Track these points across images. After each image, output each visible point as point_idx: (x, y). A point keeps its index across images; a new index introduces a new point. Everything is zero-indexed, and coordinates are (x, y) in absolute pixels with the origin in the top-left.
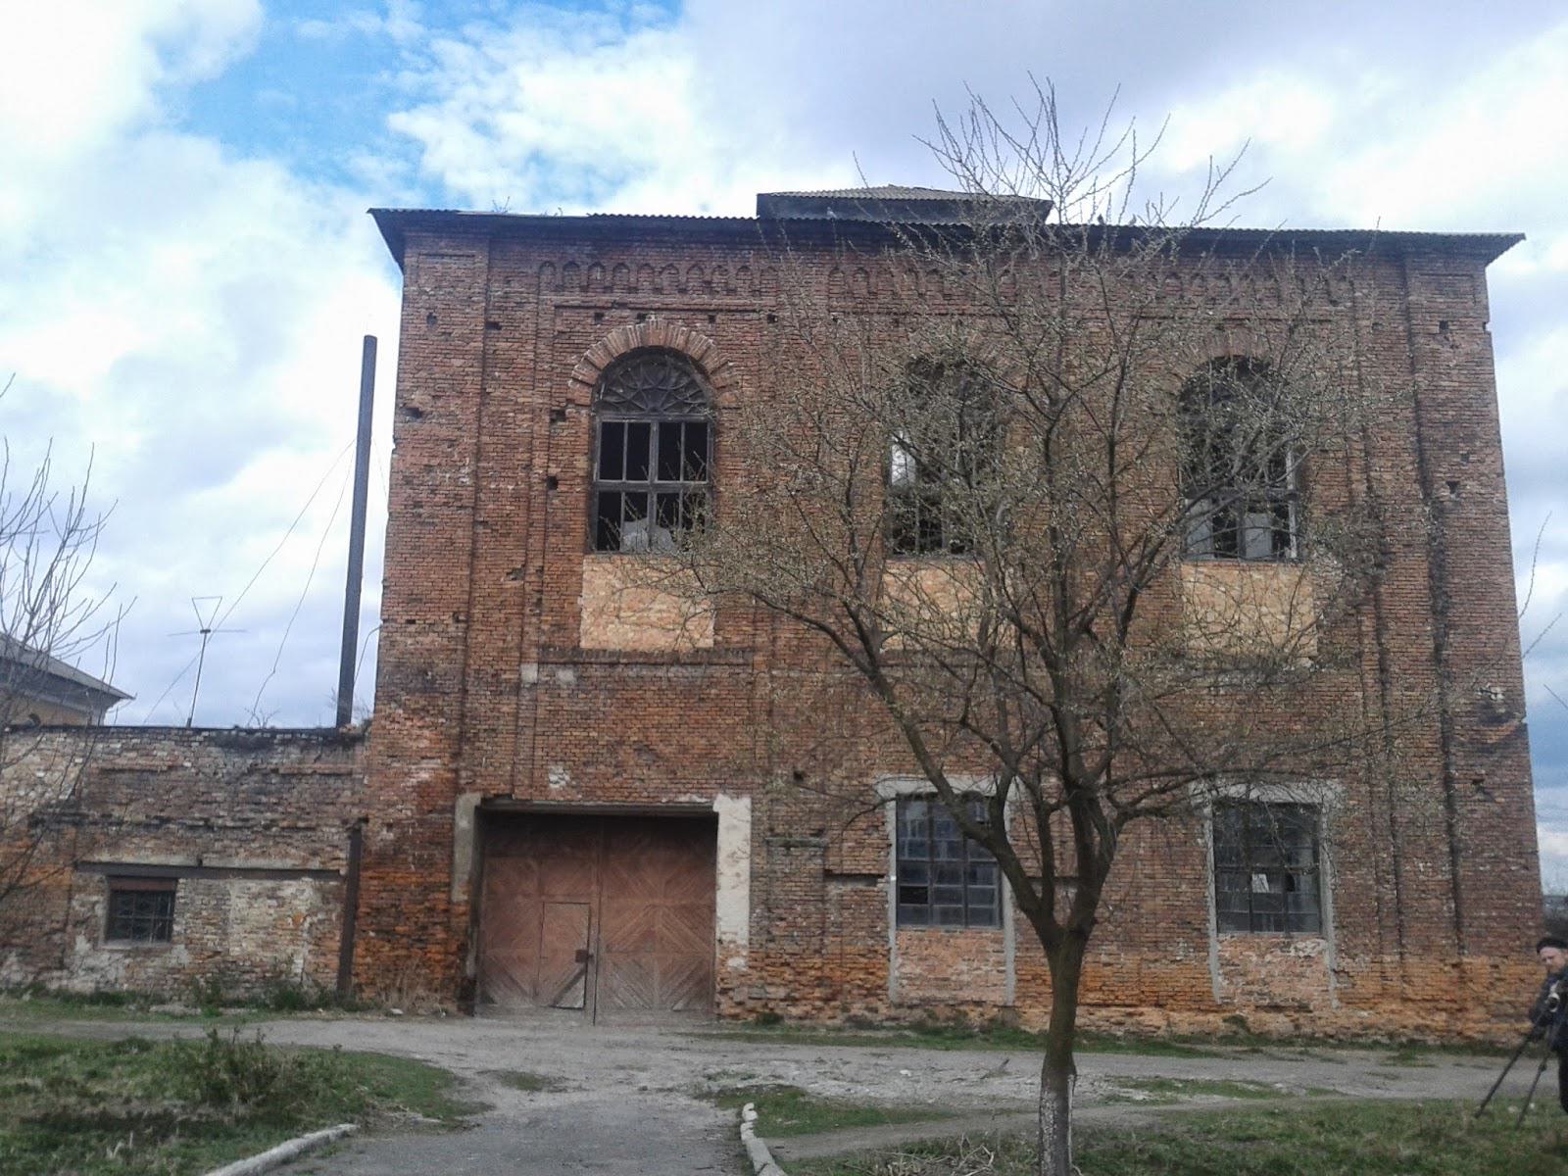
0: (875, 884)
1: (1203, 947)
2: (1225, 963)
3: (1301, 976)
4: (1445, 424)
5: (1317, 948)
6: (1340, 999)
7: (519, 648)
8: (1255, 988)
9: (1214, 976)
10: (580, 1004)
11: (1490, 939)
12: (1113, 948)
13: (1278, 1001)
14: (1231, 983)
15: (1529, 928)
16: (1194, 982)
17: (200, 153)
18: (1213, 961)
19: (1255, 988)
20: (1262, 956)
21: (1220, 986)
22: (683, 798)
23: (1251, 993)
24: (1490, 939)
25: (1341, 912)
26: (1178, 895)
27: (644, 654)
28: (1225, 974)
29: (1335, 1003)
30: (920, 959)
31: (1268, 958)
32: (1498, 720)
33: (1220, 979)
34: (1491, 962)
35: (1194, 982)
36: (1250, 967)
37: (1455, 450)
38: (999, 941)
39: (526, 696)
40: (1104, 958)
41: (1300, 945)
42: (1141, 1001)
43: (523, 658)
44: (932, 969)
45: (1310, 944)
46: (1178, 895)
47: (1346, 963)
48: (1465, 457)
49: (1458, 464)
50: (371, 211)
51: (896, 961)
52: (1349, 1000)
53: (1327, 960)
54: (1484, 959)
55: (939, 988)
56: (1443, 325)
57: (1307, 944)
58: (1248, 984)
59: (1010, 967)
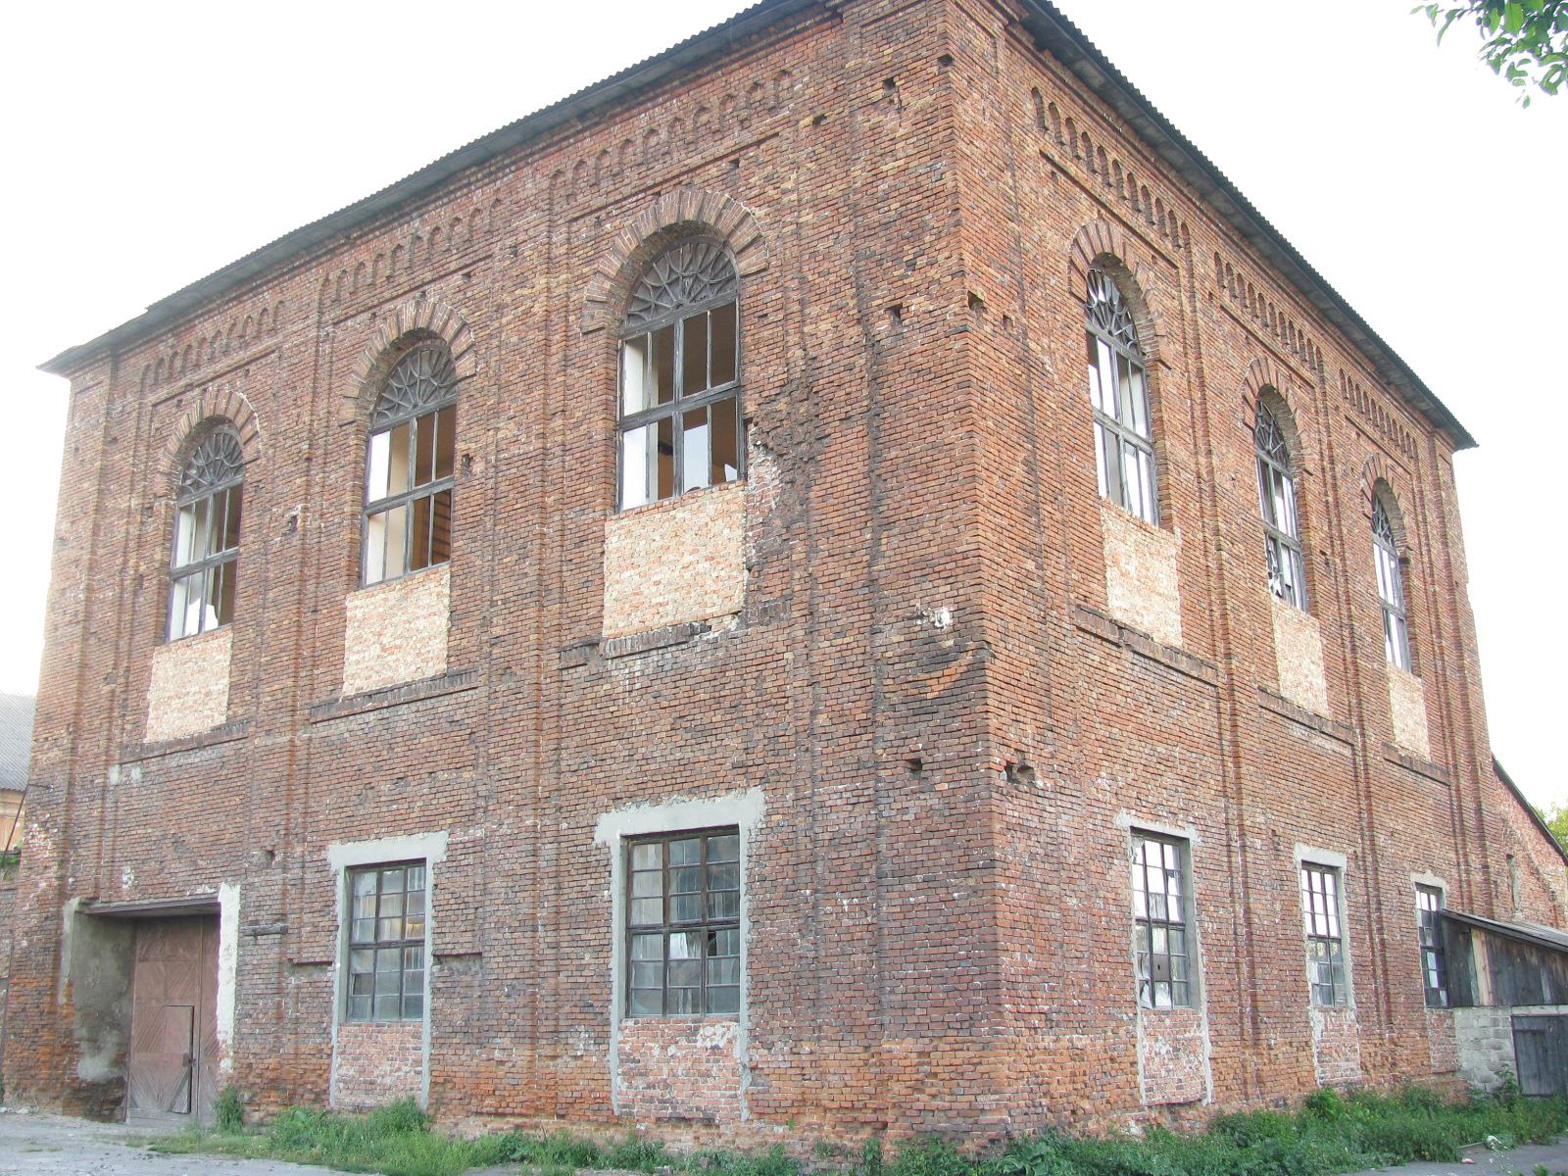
0: (326, 971)
1: (602, 1039)
2: (626, 1058)
3: (707, 1074)
4: (886, 225)
5: (726, 1034)
6: (751, 1109)
7: (107, 752)
8: (657, 1092)
9: (613, 1076)
10: (185, 1110)
11: (918, 1011)
12: (506, 1042)
13: (681, 1111)
14: (630, 1086)
15: (976, 990)
16: (593, 1085)
17: (420, 574)
18: (613, 1058)
19: (657, 1092)
20: (664, 1048)
21: (619, 1089)
22: (200, 890)
23: (651, 1100)
24: (918, 1011)
25: (758, 983)
26: (581, 968)
27: (179, 742)
28: (624, 1073)
29: (745, 1114)
30: (354, 1059)
31: (672, 1050)
32: (943, 659)
33: (619, 1078)
34: (919, 1047)
35: (593, 1085)
36: (652, 1064)
37: (896, 259)
38: (417, 1036)
39: (110, 798)
40: (497, 1054)
41: (709, 1031)
42: (537, 1109)
43: (108, 764)
44: (362, 1072)
45: (719, 1029)
46: (581, 968)
47: (760, 1055)
48: (911, 265)
49: (902, 278)
50: (41, 367)
51: (336, 1061)
52: (762, 1110)
53: (738, 1052)
54: (909, 1043)
55: (367, 1092)
56: (889, 83)
57: (716, 1031)
58: (648, 1087)
59: (425, 1067)
